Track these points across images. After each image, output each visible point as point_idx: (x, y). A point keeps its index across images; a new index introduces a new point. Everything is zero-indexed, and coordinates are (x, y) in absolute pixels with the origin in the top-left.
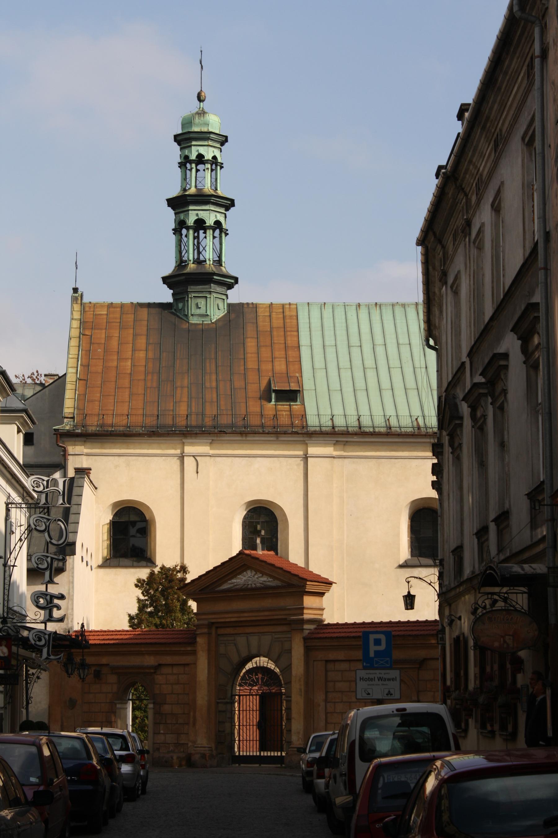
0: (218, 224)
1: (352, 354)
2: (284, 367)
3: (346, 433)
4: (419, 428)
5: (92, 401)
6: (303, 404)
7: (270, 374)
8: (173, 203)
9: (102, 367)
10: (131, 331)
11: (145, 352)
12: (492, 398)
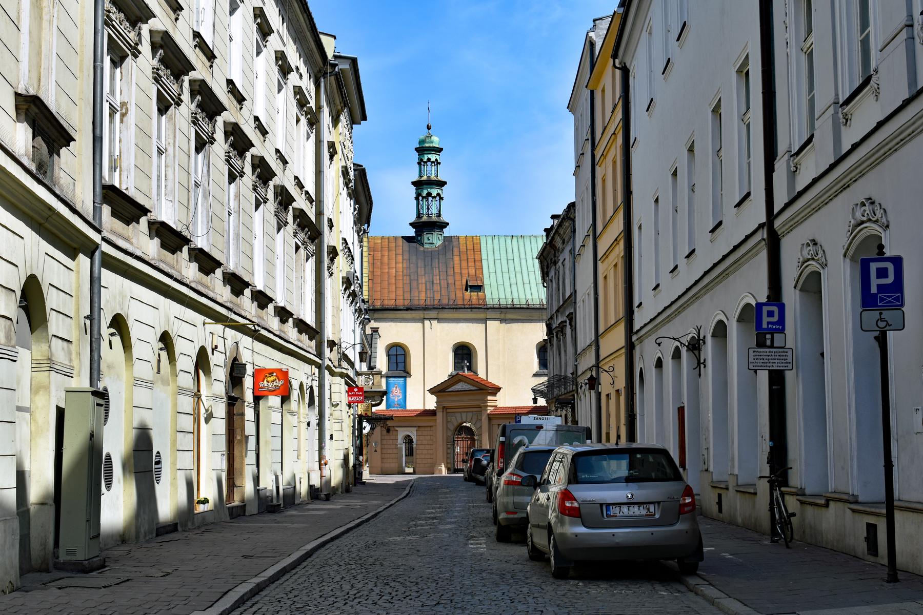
0: (438, 194)
2: (474, 271)
7: (467, 276)
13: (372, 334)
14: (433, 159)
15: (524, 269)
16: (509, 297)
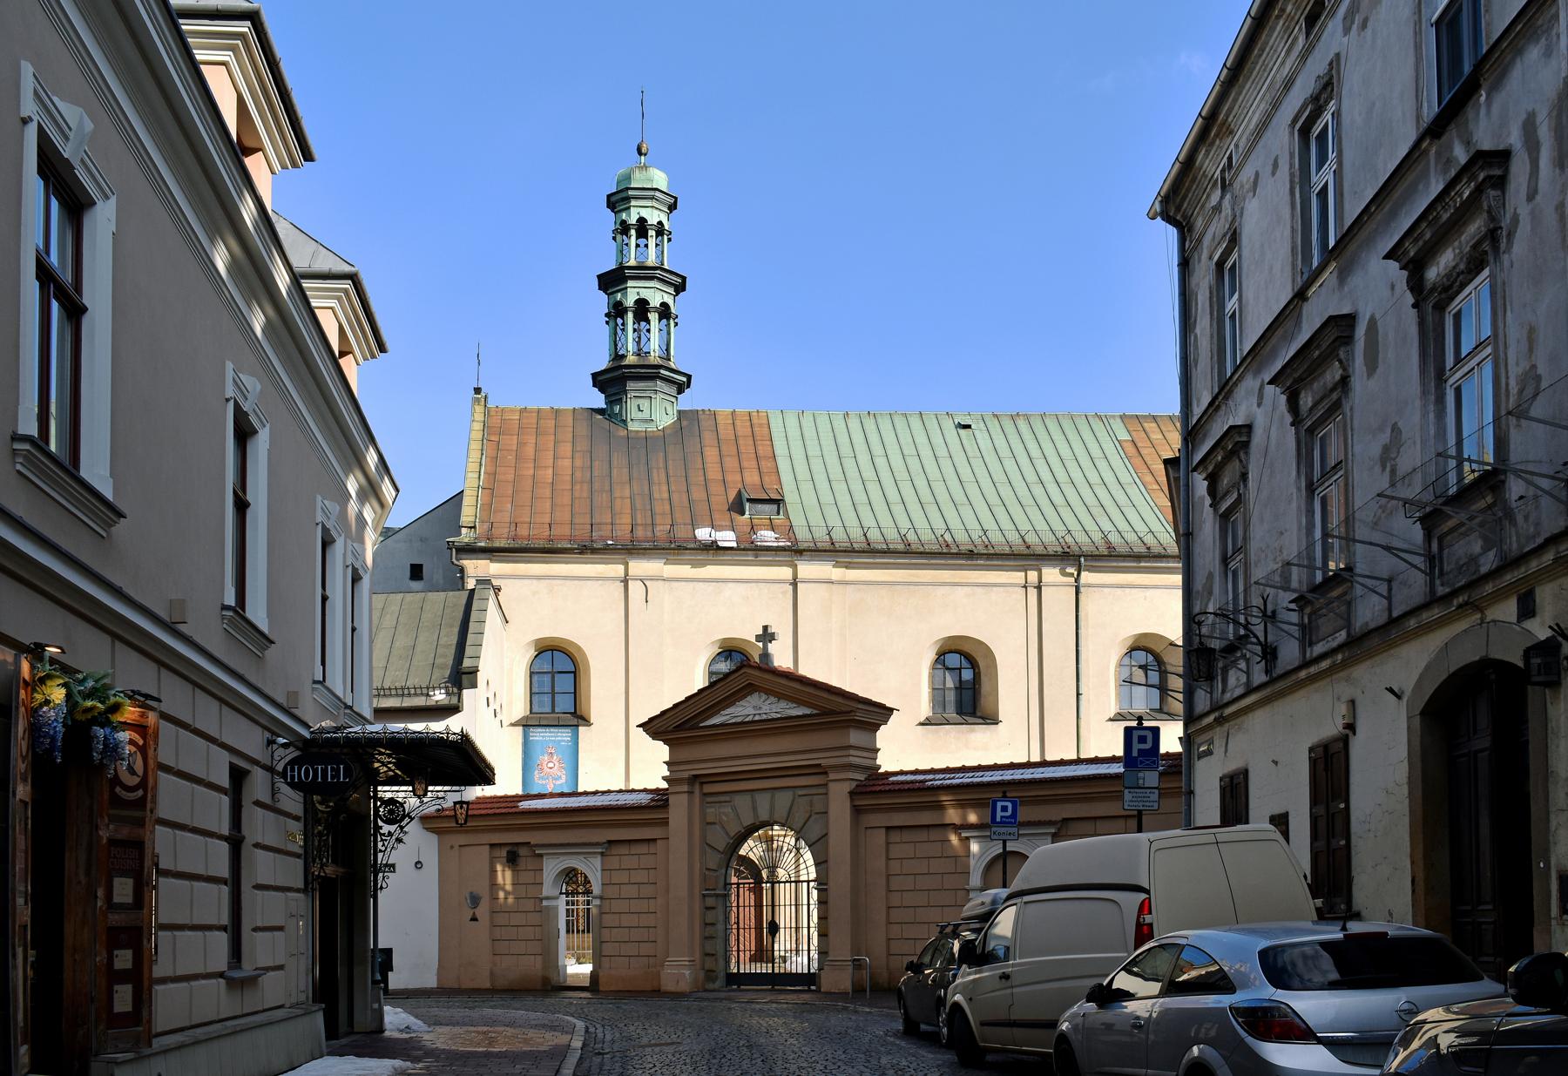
1: (844, 465)
2: (756, 479)
3: (851, 551)
7: (740, 486)
9: (513, 476)
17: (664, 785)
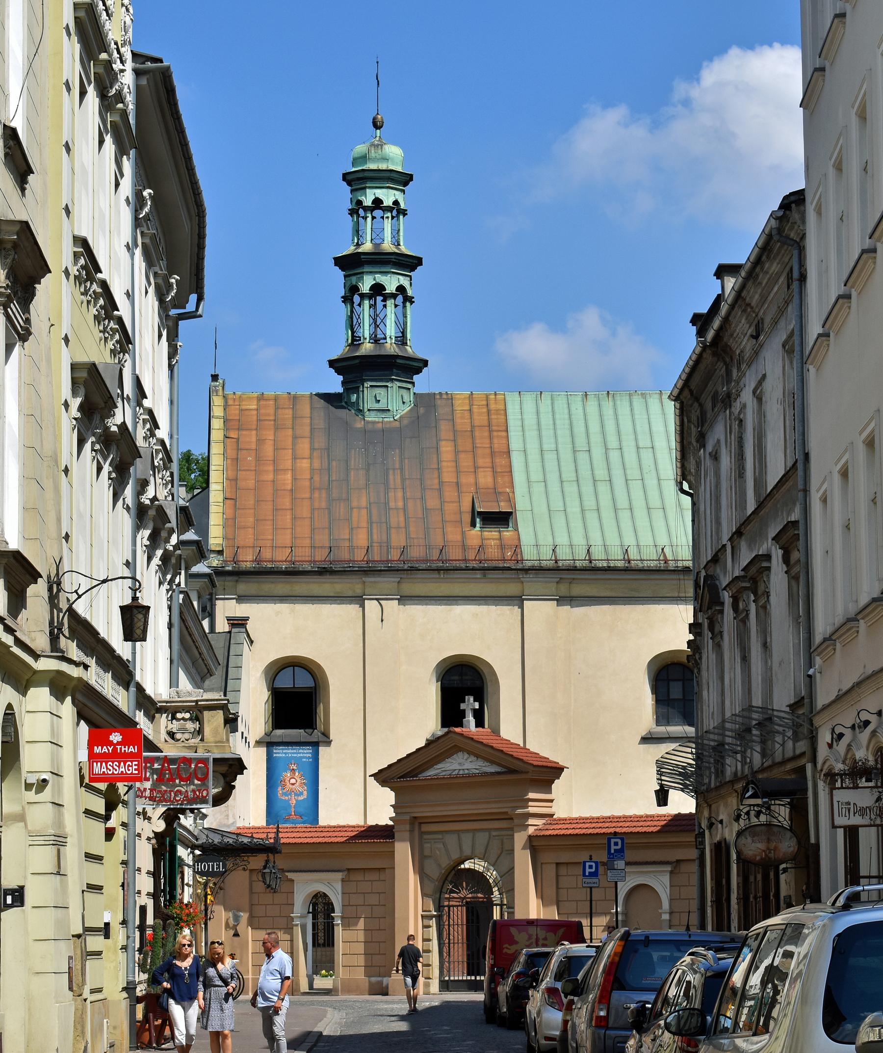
0: (401, 289)
2: (490, 480)
4: (666, 561)
5: (245, 528)
6: (516, 529)
7: (473, 489)
8: (343, 262)
10: (290, 432)
11: (309, 460)
12: (755, 596)
13: (230, 632)
14: (388, 202)
15: (617, 473)
16: (579, 540)
17: (391, 823)
